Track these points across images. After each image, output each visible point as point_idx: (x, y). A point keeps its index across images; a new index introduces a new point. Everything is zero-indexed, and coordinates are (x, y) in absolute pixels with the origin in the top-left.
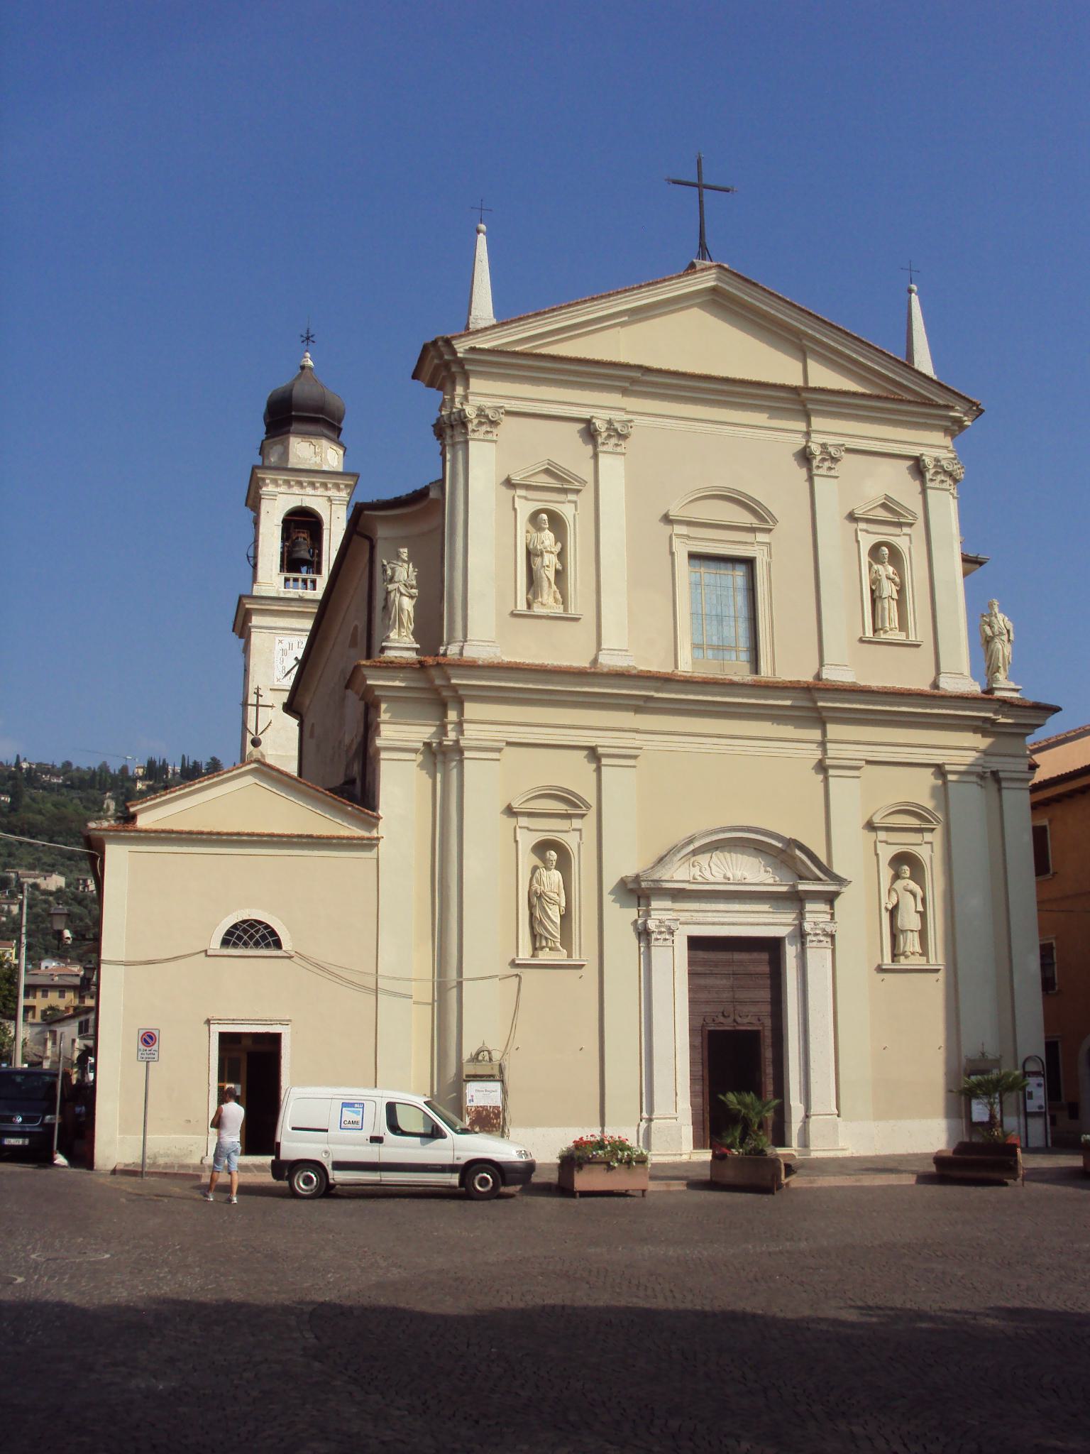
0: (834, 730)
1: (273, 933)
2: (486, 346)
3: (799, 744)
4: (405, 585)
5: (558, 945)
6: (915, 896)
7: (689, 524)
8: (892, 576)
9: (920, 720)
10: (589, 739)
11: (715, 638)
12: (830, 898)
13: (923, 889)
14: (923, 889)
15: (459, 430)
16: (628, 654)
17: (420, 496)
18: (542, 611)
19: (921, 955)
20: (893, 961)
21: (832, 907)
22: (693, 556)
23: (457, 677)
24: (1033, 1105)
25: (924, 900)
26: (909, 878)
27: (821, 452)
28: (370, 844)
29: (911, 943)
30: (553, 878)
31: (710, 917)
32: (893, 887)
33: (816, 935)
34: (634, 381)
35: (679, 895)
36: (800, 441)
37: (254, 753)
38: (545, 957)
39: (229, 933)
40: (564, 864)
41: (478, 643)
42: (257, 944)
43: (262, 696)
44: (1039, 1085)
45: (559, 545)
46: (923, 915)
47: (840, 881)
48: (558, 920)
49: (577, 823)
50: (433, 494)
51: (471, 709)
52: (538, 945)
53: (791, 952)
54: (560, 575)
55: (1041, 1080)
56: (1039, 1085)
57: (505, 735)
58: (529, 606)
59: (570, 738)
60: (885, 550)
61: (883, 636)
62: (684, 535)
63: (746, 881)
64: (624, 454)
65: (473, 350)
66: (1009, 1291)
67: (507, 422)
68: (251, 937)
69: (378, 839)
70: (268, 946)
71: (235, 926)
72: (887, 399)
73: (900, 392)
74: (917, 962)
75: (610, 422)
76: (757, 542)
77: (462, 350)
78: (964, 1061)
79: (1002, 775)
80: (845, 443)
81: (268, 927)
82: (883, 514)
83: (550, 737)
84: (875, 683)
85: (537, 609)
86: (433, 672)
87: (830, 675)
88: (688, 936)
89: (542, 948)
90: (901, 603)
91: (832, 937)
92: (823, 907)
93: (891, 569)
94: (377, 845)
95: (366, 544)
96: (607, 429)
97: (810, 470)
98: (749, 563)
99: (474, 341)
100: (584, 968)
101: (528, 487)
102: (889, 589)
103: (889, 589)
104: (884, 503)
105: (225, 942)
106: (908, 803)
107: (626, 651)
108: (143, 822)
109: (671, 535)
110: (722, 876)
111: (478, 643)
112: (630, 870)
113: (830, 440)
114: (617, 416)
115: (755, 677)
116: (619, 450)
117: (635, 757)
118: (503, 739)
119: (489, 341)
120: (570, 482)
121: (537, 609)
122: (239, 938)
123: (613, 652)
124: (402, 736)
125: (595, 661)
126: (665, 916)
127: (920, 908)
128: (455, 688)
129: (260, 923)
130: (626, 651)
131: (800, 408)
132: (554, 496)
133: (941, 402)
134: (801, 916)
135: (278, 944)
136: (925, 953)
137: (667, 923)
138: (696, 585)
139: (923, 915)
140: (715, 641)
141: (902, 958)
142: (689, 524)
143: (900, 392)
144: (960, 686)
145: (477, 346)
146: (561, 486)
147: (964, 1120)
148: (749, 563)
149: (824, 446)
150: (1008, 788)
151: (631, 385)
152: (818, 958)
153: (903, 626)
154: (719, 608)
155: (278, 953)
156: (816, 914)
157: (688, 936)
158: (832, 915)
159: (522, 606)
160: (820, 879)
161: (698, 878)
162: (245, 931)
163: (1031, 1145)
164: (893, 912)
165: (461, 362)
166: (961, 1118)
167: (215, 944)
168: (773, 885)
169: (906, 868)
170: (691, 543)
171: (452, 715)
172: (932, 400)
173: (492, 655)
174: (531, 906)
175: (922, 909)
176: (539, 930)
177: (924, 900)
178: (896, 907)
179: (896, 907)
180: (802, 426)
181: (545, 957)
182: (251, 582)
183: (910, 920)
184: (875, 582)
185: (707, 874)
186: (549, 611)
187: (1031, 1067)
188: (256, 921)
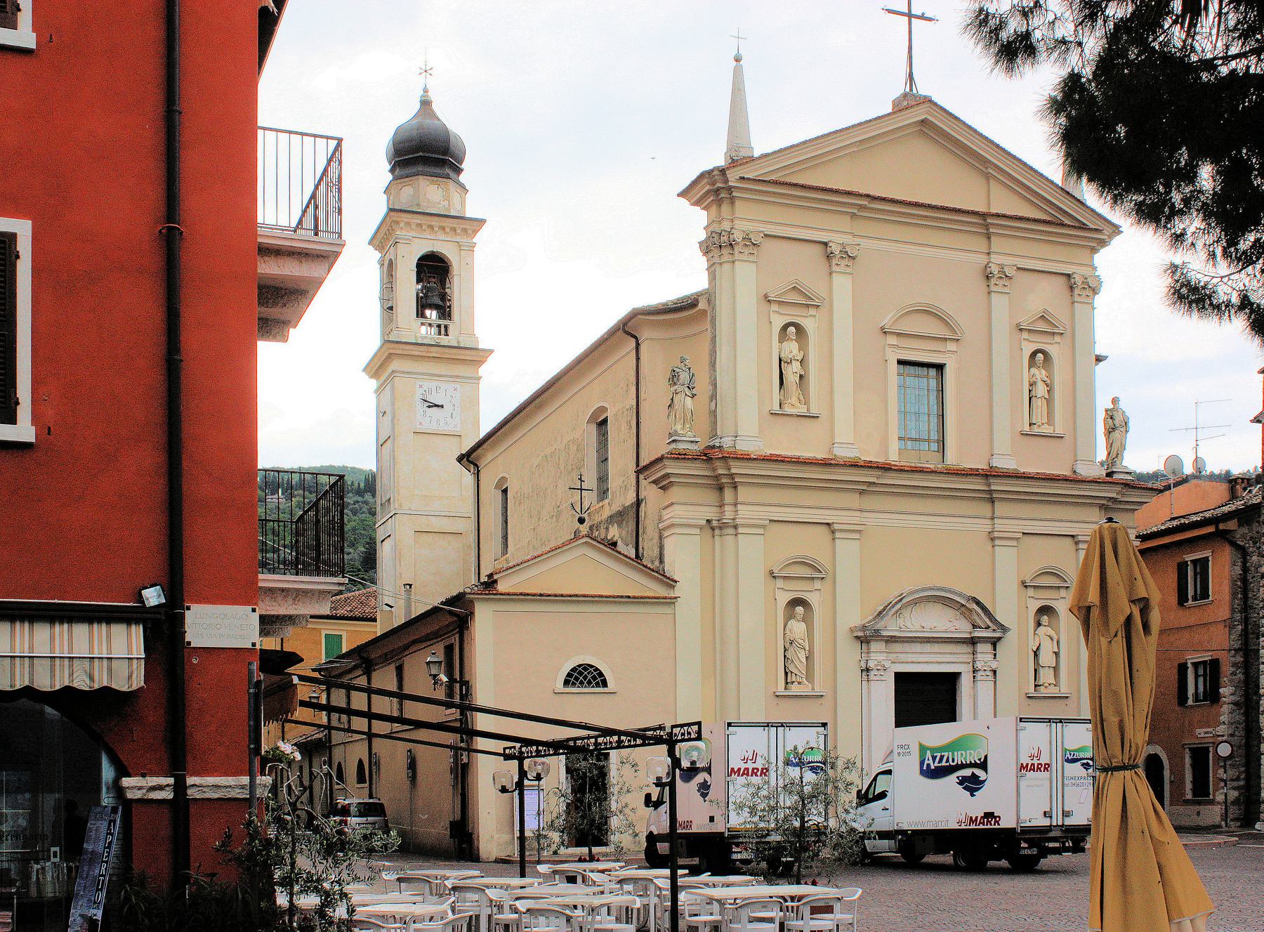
0: (1000, 508)
1: (601, 674)
2: (768, 179)
3: (942, 518)
4: (688, 387)
7: (899, 335)
8: (1045, 379)
9: (1051, 499)
12: (994, 642)
13: (1058, 633)
14: (1058, 633)
15: (725, 251)
16: (854, 447)
18: (792, 410)
19: (1055, 686)
20: (786, 688)
21: (995, 650)
22: (900, 362)
25: (1058, 642)
27: (1083, 282)
28: (670, 601)
29: (1047, 676)
30: (798, 628)
31: (910, 658)
32: (1036, 632)
34: (861, 207)
35: (892, 640)
36: (983, 259)
37: (581, 529)
38: (795, 689)
39: (569, 675)
40: (808, 620)
41: (747, 439)
42: (589, 683)
43: (584, 481)
45: (802, 353)
46: (1057, 654)
47: (1004, 629)
49: (818, 584)
50: (702, 305)
53: (965, 685)
59: (795, 515)
60: (792, 329)
62: (895, 345)
64: (852, 274)
66: (1244, 894)
67: (769, 245)
68: (585, 678)
69: (676, 598)
70: (597, 685)
71: (574, 670)
73: (1100, 224)
76: (948, 351)
80: (861, 243)
81: (597, 669)
82: (1042, 326)
83: (799, 516)
84: (1031, 469)
86: (718, 464)
88: (895, 673)
90: (1049, 401)
91: (995, 672)
92: (988, 647)
93: (1043, 372)
94: (674, 603)
98: (940, 367)
99: (742, 171)
100: (823, 698)
101: (781, 303)
102: (1041, 390)
103: (1041, 390)
104: (1043, 316)
105: (566, 683)
108: (501, 587)
109: (885, 345)
110: (919, 625)
111: (747, 439)
112: (857, 621)
113: (1007, 261)
114: (847, 239)
116: (1005, 290)
117: (860, 531)
118: (702, 517)
121: (788, 409)
122: (577, 679)
123: (843, 446)
125: (830, 451)
126: (881, 657)
128: (732, 476)
129: (591, 666)
131: (728, 196)
132: (802, 311)
135: (605, 684)
138: (902, 387)
142: (899, 335)
143: (1100, 224)
144: (1091, 471)
148: (940, 367)
149: (1002, 266)
153: (1050, 421)
155: (605, 690)
157: (895, 673)
158: (995, 655)
161: (903, 627)
162: (581, 673)
164: (1036, 654)
165: (730, 189)
167: (559, 685)
170: (900, 351)
172: (1084, 224)
173: (757, 448)
174: (785, 650)
176: (791, 668)
177: (1058, 642)
180: (981, 244)
183: (1047, 658)
185: (909, 625)
186: (797, 411)
188: (588, 665)
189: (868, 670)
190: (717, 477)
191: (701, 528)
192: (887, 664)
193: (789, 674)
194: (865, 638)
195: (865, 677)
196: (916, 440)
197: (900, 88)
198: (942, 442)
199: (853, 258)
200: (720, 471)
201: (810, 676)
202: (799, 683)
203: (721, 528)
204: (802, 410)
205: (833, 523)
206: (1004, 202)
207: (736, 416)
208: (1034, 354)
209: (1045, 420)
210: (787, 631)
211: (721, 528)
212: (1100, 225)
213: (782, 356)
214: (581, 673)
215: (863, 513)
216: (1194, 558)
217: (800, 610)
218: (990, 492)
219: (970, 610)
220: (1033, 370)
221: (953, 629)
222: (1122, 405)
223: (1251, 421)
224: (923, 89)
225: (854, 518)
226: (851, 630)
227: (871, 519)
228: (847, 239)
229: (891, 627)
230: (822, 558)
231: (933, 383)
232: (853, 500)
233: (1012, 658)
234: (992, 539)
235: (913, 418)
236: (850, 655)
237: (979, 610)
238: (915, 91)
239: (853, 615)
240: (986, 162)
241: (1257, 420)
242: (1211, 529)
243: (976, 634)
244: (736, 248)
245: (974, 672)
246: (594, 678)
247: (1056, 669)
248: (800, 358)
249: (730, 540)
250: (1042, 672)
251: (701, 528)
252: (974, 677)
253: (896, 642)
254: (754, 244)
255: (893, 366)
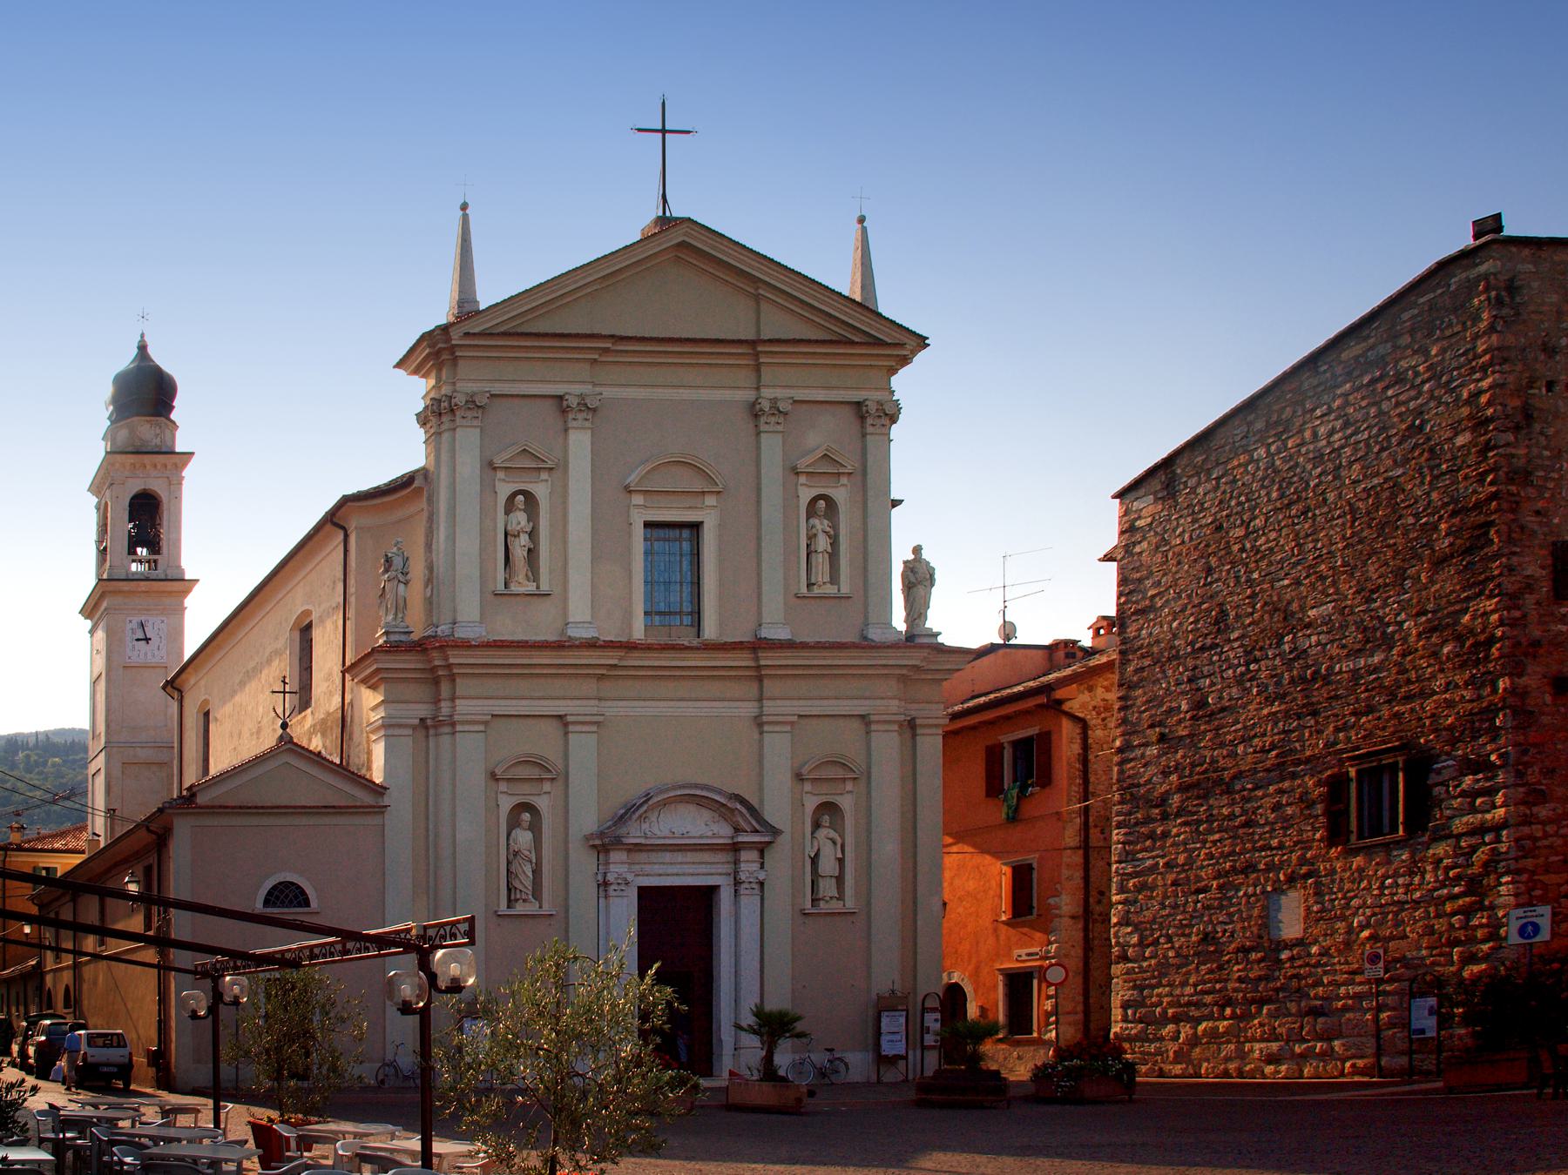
1: (303, 892)
2: (476, 330)
5: (530, 897)
6: (834, 843)
8: (828, 529)
10: (558, 709)
11: (662, 604)
12: (762, 849)
14: (842, 837)
17: (404, 485)
19: (838, 899)
20: (508, 907)
22: (647, 525)
23: (455, 656)
24: (929, 1040)
26: (829, 827)
27: (770, 408)
29: (828, 888)
33: (619, 884)
38: (520, 908)
39: (270, 893)
40: (535, 828)
44: (936, 1020)
46: (841, 861)
47: (776, 832)
48: (530, 874)
51: (462, 686)
52: (513, 897)
53: (725, 896)
54: (532, 553)
55: (938, 1015)
56: (936, 1020)
57: (490, 708)
58: (506, 585)
60: (822, 503)
61: (816, 591)
63: (690, 835)
65: (467, 334)
68: (287, 896)
69: (386, 806)
70: (300, 905)
72: (831, 342)
74: (836, 906)
75: (582, 396)
77: (456, 337)
78: (874, 997)
79: (918, 722)
85: (514, 588)
87: (766, 633)
88: (639, 887)
89: (517, 900)
90: (833, 556)
91: (762, 884)
95: (341, 536)
96: (578, 404)
97: (863, 427)
98: (696, 527)
102: (822, 543)
103: (822, 543)
106: (530, 755)
107: (590, 623)
114: (586, 389)
115: (700, 640)
119: (478, 325)
120: (544, 461)
121: (514, 588)
122: (277, 898)
124: (581, 710)
126: (623, 869)
127: (840, 855)
128: (449, 666)
130: (590, 623)
133: (857, 340)
134: (736, 862)
136: (841, 897)
137: (624, 876)
139: (841, 861)
140: (662, 607)
141: (822, 904)
145: (471, 331)
146: (1375, 764)
147: (871, 1053)
148: (696, 527)
149: (774, 401)
150: (923, 735)
151: (600, 355)
152: (749, 903)
153: (834, 579)
154: (667, 575)
156: (749, 864)
157: (639, 887)
159: (500, 587)
160: (757, 831)
163: (589, 619)
164: (815, 861)
166: (868, 1051)
168: (711, 838)
169: (827, 817)
171: (445, 689)
174: (509, 863)
175: (840, 855)
176: (516, 884)
178: (817, 855)
179: (817, 855)
181: (520, 908)
182: (182, 583)
183: (828, 866)
184: (811, 537)
185: (656, 831)
187: (929, 1004)
189: (606, 884)
190: (433, 669)
191: (414, 728)
192: (630, 877)
193: (513, 891)
194: (605, 844)
195: (602, 894)
196: (670, 613)
197: (653, 211)
198: (697, 614)
199: (594, 410)
200: (437, 663)
201: (537, 893)
202: (524, 901)
203: (435, 727)
204: (531, 587)
205: (566, 715)
206: (776, 324)
207: (454, 600)
208: (814, 500)
209: (827, 579)
210: (511, 842)
211: (435, 727)
212: (903, 338)
213: (509, 528)
214: (282, 892)
215: (603, 703)
216: (1011, 739)
217: (526, 816)
218: (759, 667)
219: (732, 810)
220: (812, 521)
221: (710, 834)
222: (925, 555)
223: (1100, 560)
224: (677, 211)
225: (590, 707)
226: (587, 838)
227: (613, 709)
228: (586, 389)
229: (634, 833)
230: (552, 754)
231: (686, 546)
232: (590, 687)
233: (782, 868)
234: (760, 725)
235: (662, 588)
236: (584, 865)
237: (744, 810)
238: (668, 214)
239: (587, 818)
240: (756, 280)
241: (1108, 558)
242: (1043, 699)
243: (740, 839)
244: (458, 413)
245: (735, 885)
246: (296, 897)
247: (840, 880)
248: (529, 530)
249: (445, 740)
250: (822, 883)
251: (414, 728)
252: (736, 891)
253: (641, 851)
254: (479, 407)
255: (639, 531)
